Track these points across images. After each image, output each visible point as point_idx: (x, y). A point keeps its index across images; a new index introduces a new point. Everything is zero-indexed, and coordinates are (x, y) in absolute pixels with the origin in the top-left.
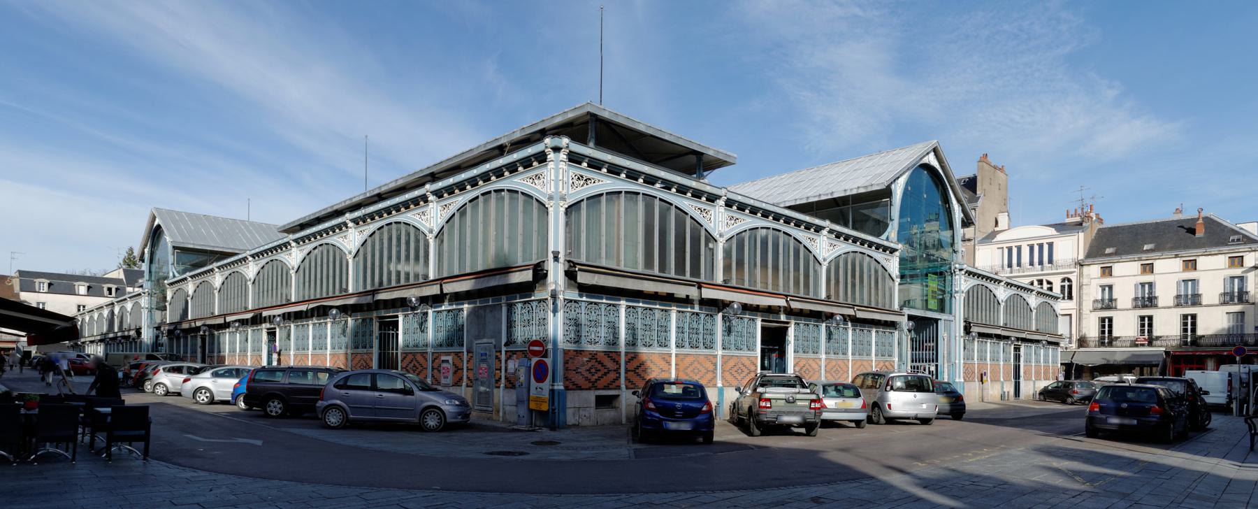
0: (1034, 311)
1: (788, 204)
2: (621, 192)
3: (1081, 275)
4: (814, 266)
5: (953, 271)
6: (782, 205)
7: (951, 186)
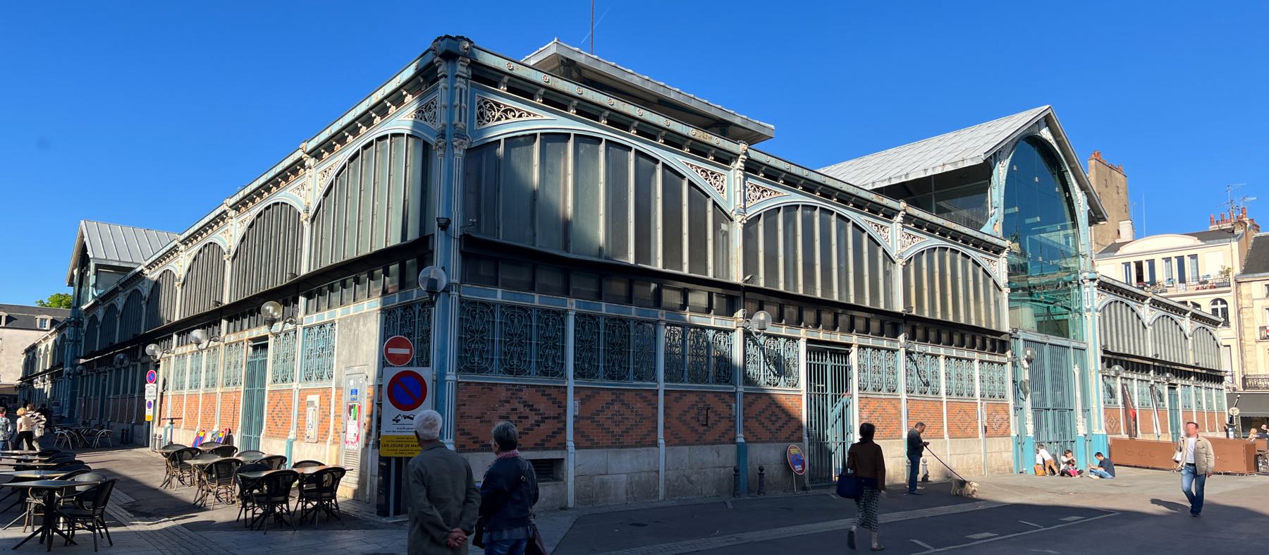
0: (1149, 329)
1: (878, 186)
2: (935, 248)
3: (1238, 295)
4: (994, 294)
5: (1080, 282)
6: (870, 187)
7: (1071, 169)
